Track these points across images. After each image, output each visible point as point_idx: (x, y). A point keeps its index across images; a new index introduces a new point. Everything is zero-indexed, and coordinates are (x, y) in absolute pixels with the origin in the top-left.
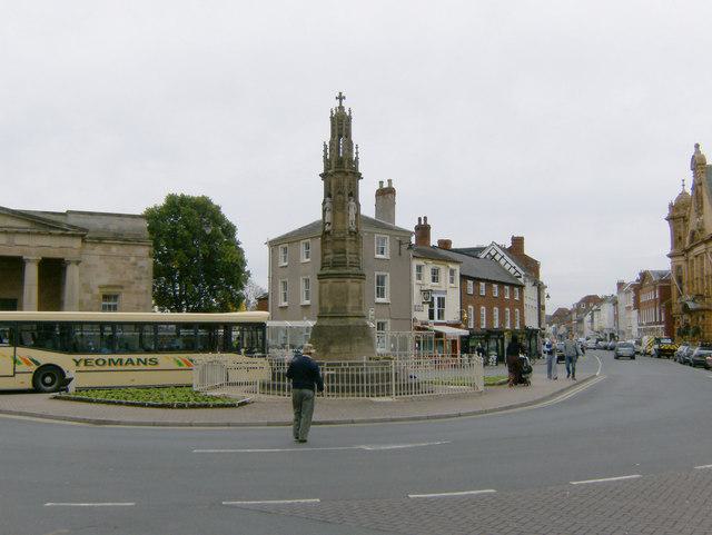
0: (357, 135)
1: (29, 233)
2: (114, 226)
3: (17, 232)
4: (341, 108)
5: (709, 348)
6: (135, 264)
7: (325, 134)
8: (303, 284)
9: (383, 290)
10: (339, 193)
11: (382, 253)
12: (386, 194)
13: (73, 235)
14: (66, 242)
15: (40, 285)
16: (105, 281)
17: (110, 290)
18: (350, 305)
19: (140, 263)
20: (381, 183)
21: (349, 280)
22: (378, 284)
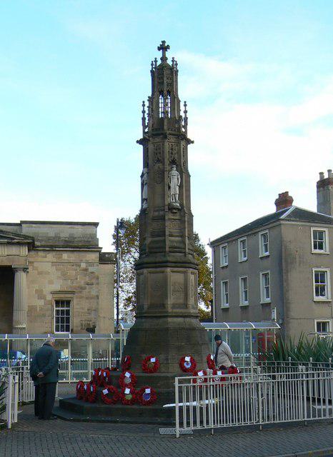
0: (186, 89)
2: (65, 233)
4: (164, 59)
5: (2, 362)
6: (86, 270)
7: (144, 87)
8: (241, 284)
9: (323, 289)
10: (159, 161)
11: (321, 248)
13: (19, 244)
14: (14, 250)
16: (57, 287)
17: (62, 296)
18: (171, 301)
19: (91, 269)
20: (321, 174)
21: (169, 270)
22: (317, 282)
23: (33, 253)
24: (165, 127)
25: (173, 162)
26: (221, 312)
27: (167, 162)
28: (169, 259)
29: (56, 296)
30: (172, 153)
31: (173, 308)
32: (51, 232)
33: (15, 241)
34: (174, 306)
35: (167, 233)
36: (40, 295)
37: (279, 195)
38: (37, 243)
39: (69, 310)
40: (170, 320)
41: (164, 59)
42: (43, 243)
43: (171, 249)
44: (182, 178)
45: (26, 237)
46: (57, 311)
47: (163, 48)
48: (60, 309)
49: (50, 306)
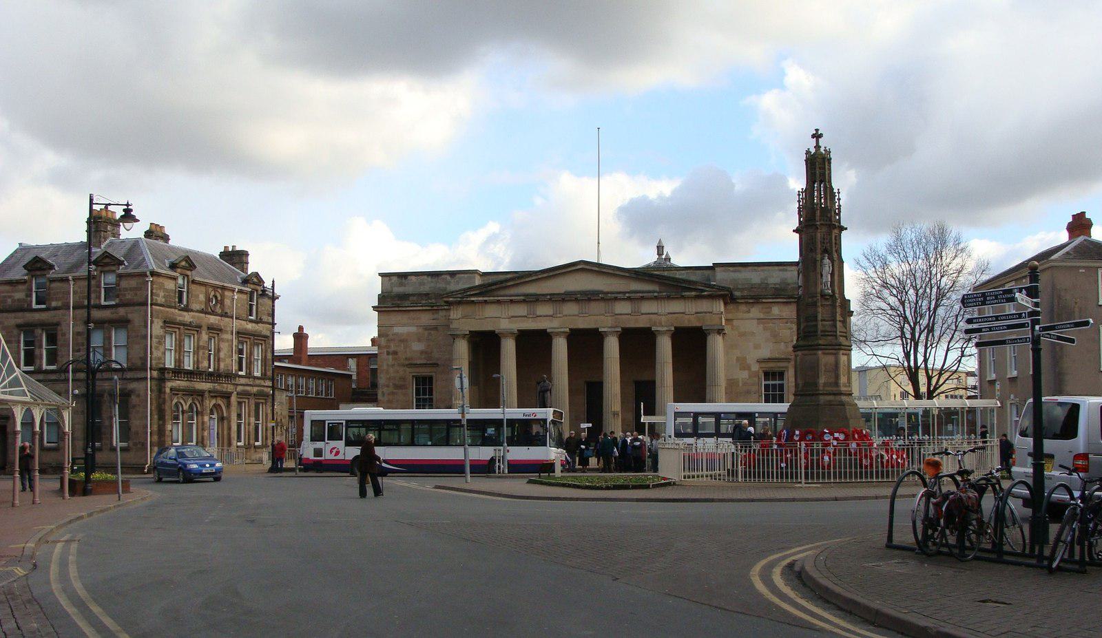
1: (656, 298)
3: (642, 298)
12: (300, 337)
13: (711, 297)
14: (704, 305)
15: (622, 382)
16: (765, 353)
17: (771, 365)
18: (822, 380)
21: (820, 352)
23: (731, 307)
24: (817, 218)
25: (825, 251)
26: (1008, 382)
27: (819, 251)
28: (820, 342)
29: (763, 365)
30: (824, 243)
31: (824, 386)
32: (755, 277)
33: (705, 293)
34: (825, 385)
35: (820, 317)
36: (744, 366)
37: (1073, 216)
38: (737, 294)
39: (238, 420)
40: (821, 397)
41: (817, 147)
42: (745, 293)
43: (823, 333)
44: (833, 265)
45: (723, 288)
46: (767, 387)
47: (817, 136)
48: (771, 382)
49: (756, 379)
